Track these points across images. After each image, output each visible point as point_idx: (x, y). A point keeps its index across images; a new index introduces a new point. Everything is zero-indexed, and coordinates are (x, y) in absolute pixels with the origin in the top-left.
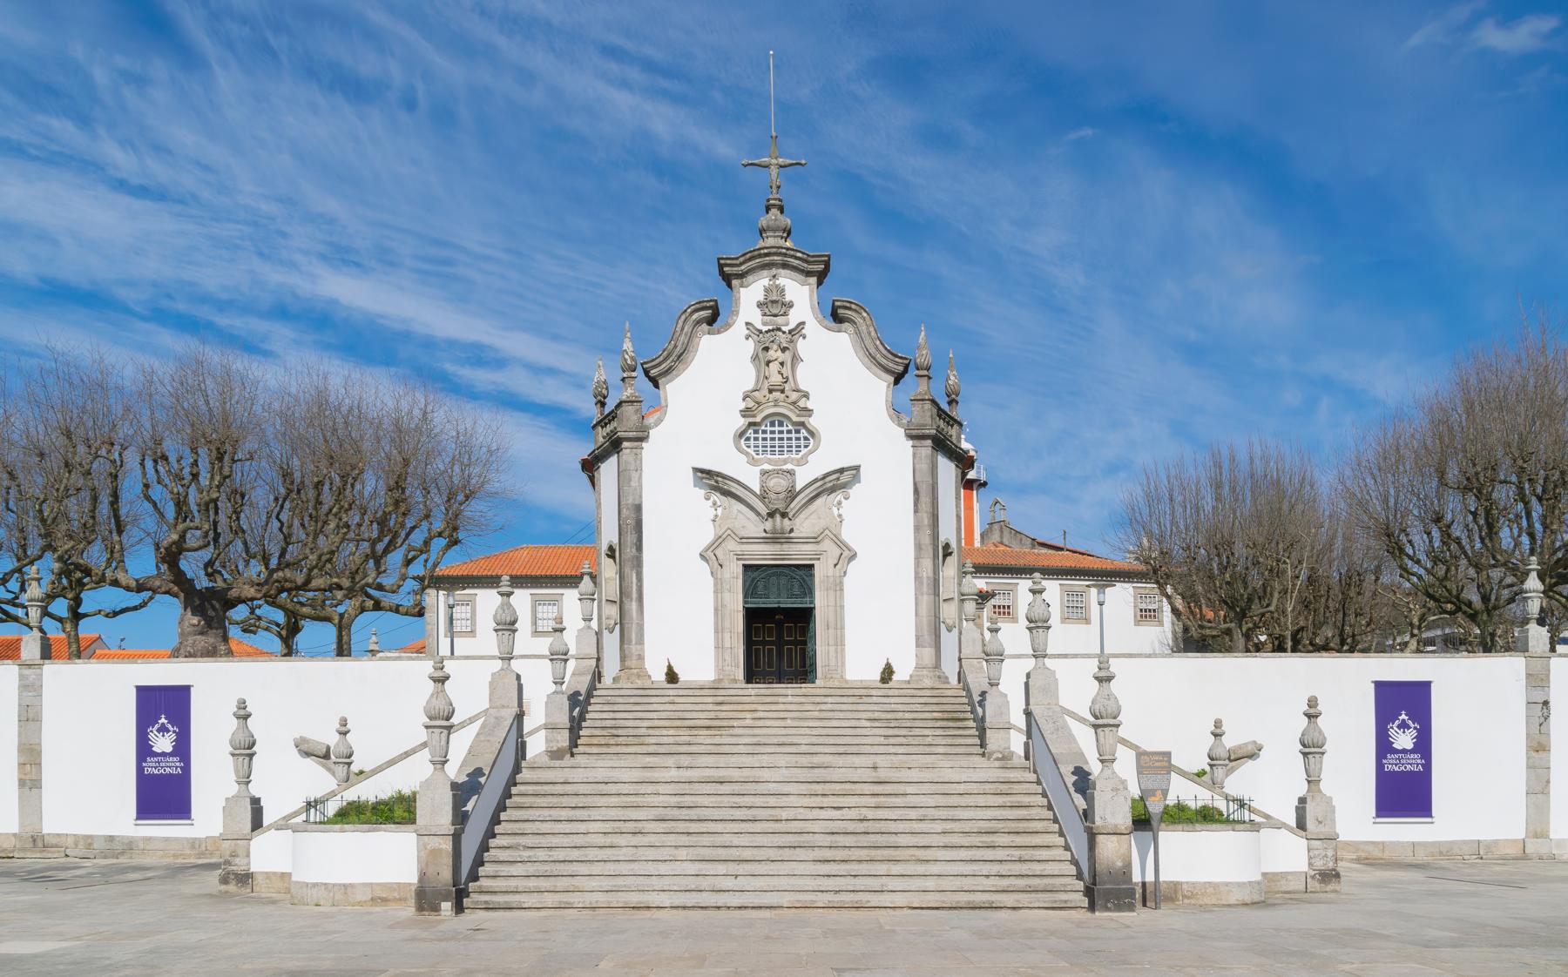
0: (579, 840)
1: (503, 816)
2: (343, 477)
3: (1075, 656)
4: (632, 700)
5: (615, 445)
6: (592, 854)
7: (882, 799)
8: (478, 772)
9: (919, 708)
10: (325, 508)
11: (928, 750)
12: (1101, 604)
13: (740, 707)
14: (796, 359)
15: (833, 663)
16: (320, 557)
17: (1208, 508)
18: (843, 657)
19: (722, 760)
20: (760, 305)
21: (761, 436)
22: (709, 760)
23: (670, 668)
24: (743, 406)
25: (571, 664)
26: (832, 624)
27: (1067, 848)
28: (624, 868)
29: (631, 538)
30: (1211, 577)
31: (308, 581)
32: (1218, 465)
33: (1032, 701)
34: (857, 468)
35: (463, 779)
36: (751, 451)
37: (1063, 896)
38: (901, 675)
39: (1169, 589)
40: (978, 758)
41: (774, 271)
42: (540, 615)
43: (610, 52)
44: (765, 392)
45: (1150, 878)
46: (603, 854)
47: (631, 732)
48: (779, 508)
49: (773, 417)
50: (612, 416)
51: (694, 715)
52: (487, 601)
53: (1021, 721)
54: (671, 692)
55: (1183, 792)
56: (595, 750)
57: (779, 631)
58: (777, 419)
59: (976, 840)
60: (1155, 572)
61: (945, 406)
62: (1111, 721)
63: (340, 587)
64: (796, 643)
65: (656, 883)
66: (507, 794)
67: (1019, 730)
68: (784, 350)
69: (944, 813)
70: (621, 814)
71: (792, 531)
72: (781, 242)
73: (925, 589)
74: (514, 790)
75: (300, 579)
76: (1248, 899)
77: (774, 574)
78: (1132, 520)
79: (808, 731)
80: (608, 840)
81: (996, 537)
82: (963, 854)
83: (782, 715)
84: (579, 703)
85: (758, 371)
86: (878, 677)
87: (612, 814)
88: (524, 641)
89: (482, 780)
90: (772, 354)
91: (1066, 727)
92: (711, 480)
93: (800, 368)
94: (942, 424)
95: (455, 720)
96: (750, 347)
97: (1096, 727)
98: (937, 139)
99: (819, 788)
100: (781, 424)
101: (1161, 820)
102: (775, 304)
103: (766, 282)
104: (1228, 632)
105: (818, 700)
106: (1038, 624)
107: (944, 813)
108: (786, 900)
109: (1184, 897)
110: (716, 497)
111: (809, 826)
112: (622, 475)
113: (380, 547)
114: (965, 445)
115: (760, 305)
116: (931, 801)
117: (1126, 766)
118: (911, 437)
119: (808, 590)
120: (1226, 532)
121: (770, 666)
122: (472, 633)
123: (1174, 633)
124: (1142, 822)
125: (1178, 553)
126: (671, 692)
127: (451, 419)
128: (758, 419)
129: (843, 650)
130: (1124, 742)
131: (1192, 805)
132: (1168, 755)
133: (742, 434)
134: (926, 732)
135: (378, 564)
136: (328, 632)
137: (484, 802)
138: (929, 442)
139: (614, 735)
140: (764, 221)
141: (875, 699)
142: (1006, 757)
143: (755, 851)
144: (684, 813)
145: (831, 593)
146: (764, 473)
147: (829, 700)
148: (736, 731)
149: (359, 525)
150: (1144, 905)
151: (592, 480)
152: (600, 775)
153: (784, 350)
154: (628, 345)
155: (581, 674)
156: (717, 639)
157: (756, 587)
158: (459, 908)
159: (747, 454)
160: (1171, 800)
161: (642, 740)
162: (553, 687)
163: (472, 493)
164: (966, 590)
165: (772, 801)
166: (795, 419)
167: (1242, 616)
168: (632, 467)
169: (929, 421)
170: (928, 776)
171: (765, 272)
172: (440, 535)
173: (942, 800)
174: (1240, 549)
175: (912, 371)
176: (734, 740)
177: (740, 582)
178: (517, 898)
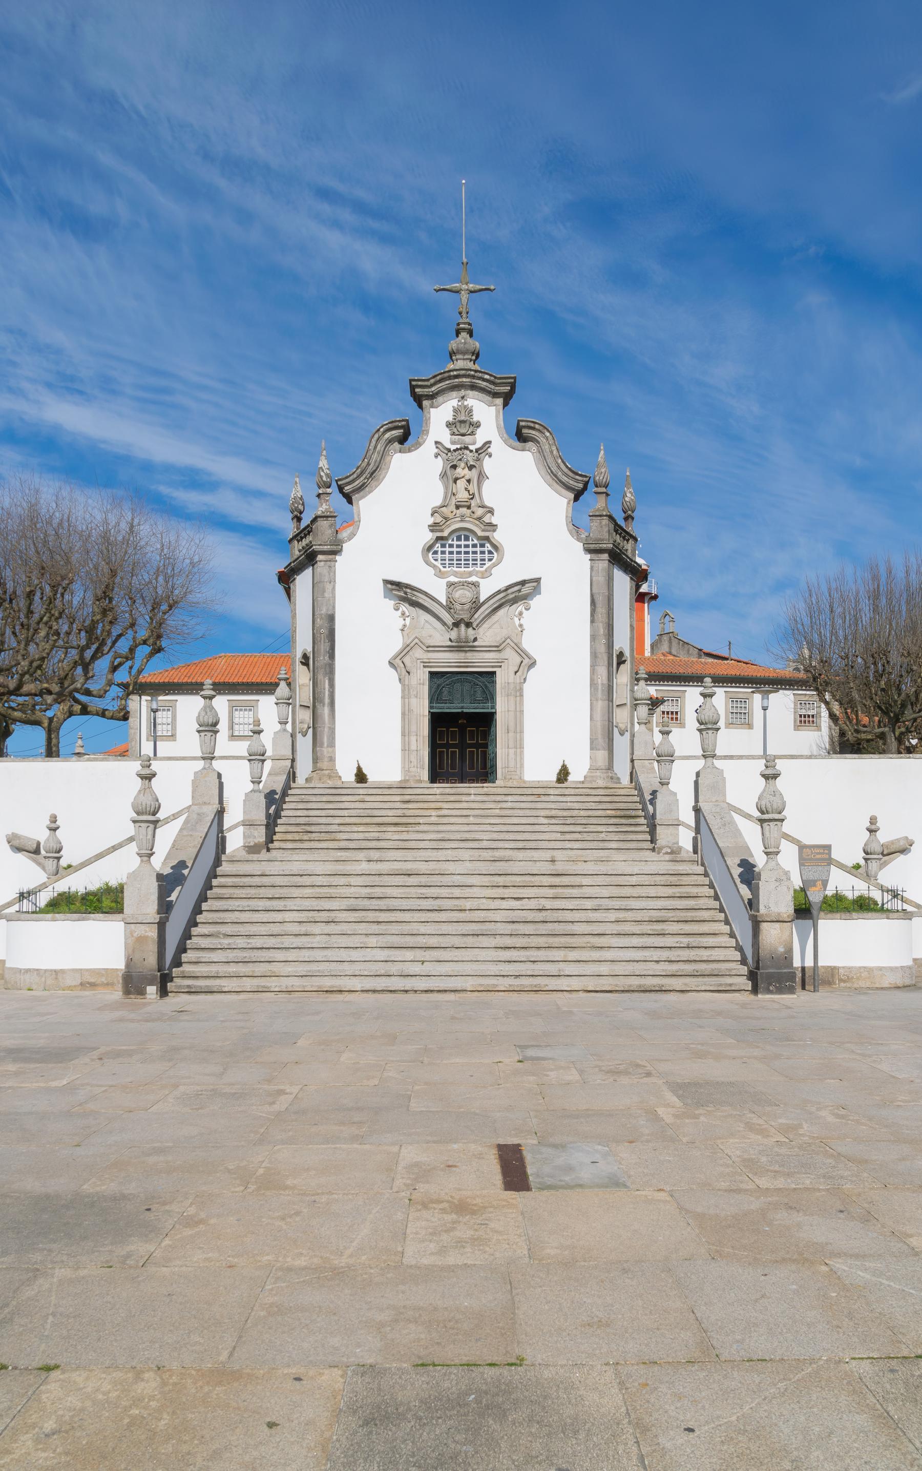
0: (275, 929)
1: (204, 906)
2: (54, 587)
3: (741, 757)
4: (324, 799)
5: (310, 558)
6: (288, 941)
7: (560, 890)
8: (182, 864)
9: (593, 806)
10: (36, 617)
11: (601, 845)
12: (765, 709)
14: (482, 476)
15: (512, 764)
16: (31, 663)
17: (865, 620)
18: (522, 759)
19: (409, 855)
20: (449, 425)
21: (447, 549)
22: (399, 855)
23: (359, 769)
24: (431, 521)
25: (268, 765)
26: (512, 728)
27: (732, 935)
28: (319, 955)
29: (324, 646)
30: (867, 685)
31: (20, 686)
32: (875, 578)
33: (701, 798)
34: (538, 580)
35: (167, 871)
36: (438, 564)
37: (729, 980)
38: (577, 775)
39: (827, 696)
40: (648, 853)
41: (463, 392)
42: (236, 720)
43: (324, 194)
45: (809, 963)
46: (298, 942)
47: (323, 828)
48: (464, 617)
49: (461, 531)
50: (307, 531)
52: (189, 707)
53: (688, 817)
54: (361, 791)
55: (842, 883)
56: (289, 845)
57: (462, 735)
58: (463, 534)
59: (647, 928)
60: (815, 679)
61: (622, 523)
62: (777, 816)
63: (49, 692)
64: (477, 746)
65: (348, 968)
66: (208, 886)
67: (687, 826)
68: (471, 468)
69: (617, 904)
70: (315, 904)
71: (475, 640)
72: (470, 365)
73: (600, 695)
74: (215, 882)
75: (12, 684)
76: (900, 983)
77: (459, 681)
78: (796, 633)
79: (489, 828)
80: (303, 929)
81: (665, 647)
82: (635, 941)
83: (465, 812)
84: (275, 801)
85: (446, 488)
87: (307, 904)
88: (223, 744)
89: (186, 872)
90: (460, 471)
91: (732, 822)
92: (401, 592)
93: (486, 485)
94: (618, 538)
95: (161, 815)
97: (762, 821)
98: (627, 278)
99: (500, 880)
100: (467, 538)
101: (821, 909)
102: (463, 424)
103: (454, 403)
104: (882, 736)
106: (707, 726)
107: (617, 904)
108: (469, 983)
109: (841, 980)
110: (404, 607)
111: (491, 916)
112: (315, 585)
113: (88, 654)
114: (639, 560)
115: (449, 425)
116: (605, 892)
117: (789, 858)
118: (589, 551)
119: (490, 696)
120: (882, 641)
122: (173, 737)
123: (831, 738)
124: (803, 911)
125: (838, 663)
126: (361, 791)
127: (154, 535)
128: (445, 534)
129: (522, 753)
130: (786, 837)
131: (850, 895)
132: (828, 848)
133: (430, 548)
134: (600, 828)
135: (86, 667)
136: (38, 735)
137: (187, 894)
139: (307, 833)
140: (454, 344)
141: (552, 798)
142: (675, 851)
143: (441, 939)
144: (375, 904)
145: (512, 699)
146: (450, 585)
147: (510, 798)
148: (421, 828)
149: (68, 634)
150: (803, 988)
151: (288, 592)
152: (295, 868)
153: (471, 468)
154: (323, 463)
155: (276, 774)
157: (441, 693)
158: (164, 992)
159: (434, 567)
160: (830, 891)
161: (333, 836)
162: (251, 786)
163: (176, 602)
164: (639, 695)
165: (457, 892)
166: (480, 533)
167: (896, 720)
168: (326, 579)
169: (606, 536)
170: (602, 868)
171: (454, 394)
172: (145, 642)
174: (895, 658)
175: (591, 488)
176: (420, 836)
177: (426, 688)
178: (217, 982)
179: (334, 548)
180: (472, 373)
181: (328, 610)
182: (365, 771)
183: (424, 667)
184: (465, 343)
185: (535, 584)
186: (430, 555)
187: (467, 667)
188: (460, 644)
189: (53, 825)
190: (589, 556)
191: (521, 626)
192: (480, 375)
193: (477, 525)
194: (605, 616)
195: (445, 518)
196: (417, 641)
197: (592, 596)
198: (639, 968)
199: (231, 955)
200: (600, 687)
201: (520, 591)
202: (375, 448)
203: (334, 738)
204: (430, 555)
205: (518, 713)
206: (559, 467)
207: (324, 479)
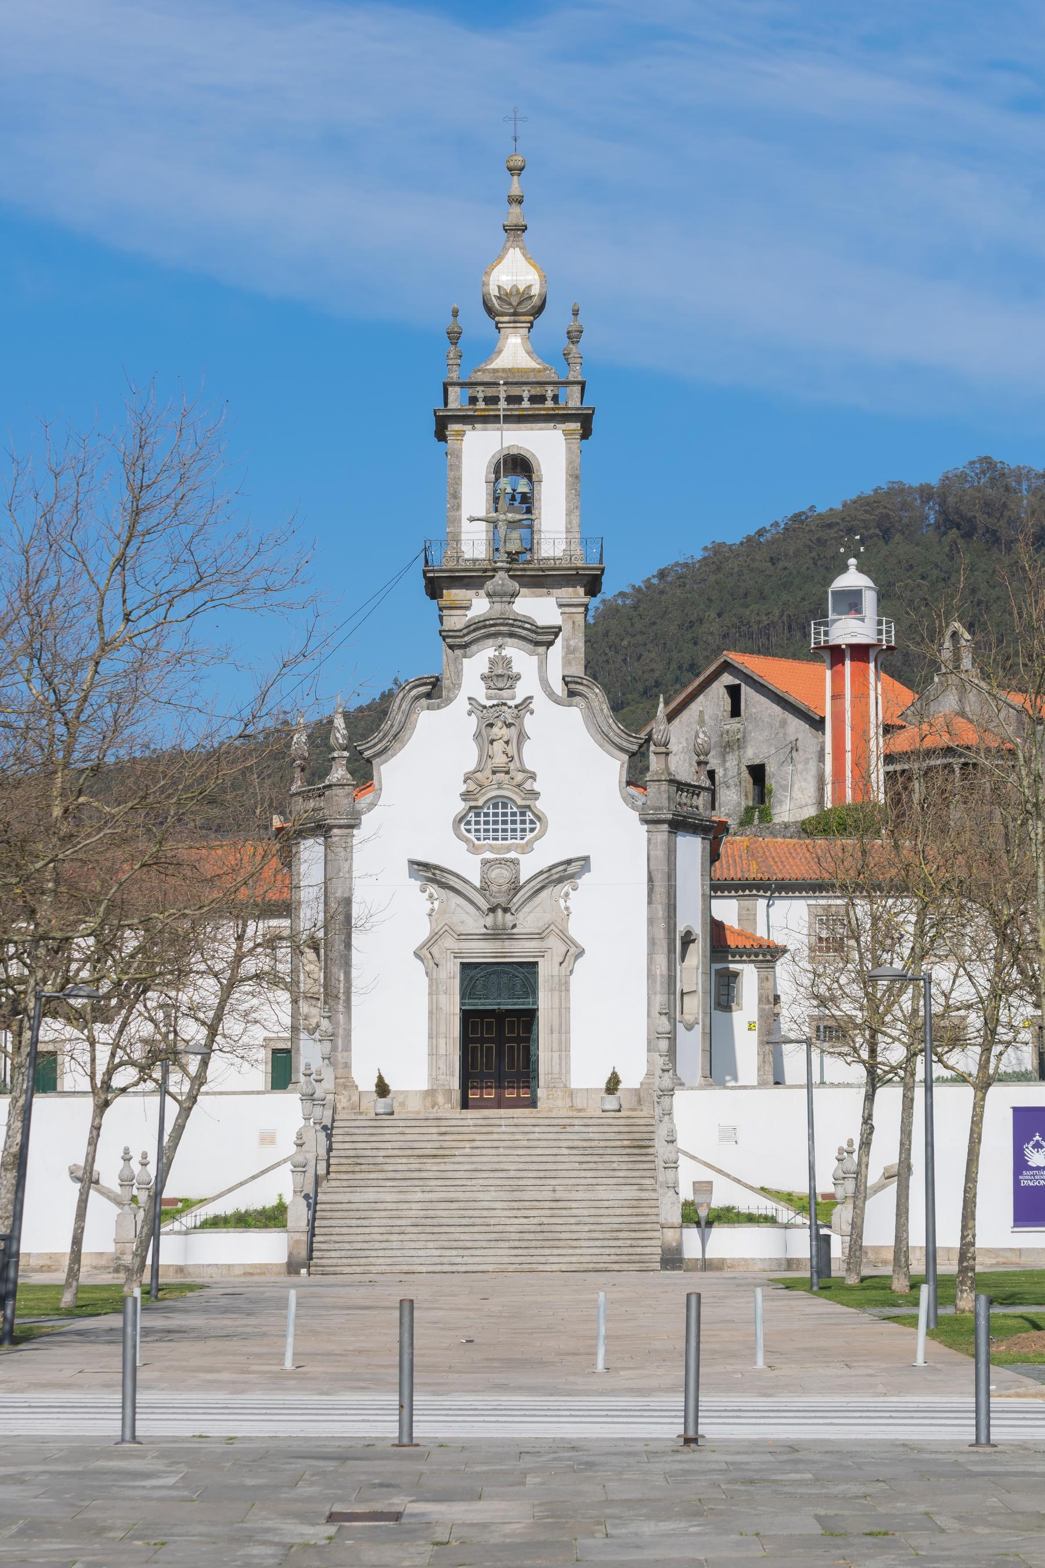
0: (367, 1238)
4: (368, 1131)
7: (556, 1211)
9: (612, 1136)
13: (460, 1137)
14: (522, 737)
15: (556, 1070)
18: (568, 1064)
20: (484, 678)
23: (380, 1078)
24: (463, 788)
26: (556, 1028)
38: (631, 1080)
41: (500, 640)
44: (488, 772)
48: (502, 900)
51: (423, 1145)
57: (498, 1037)
59: (607, 1235)
64: (518, 1040)
71: (514, 926)
73: (658, 988)
79: (517, 1159)
83: (495, 1144)
85: (481, 750)
86: (603, 1085)
87: (384, 1222)
92: (428, 873)
93: (527, 747)
96: (472, 723)
99: (515, 1205)
102: (500, 677)
105: (527, 1129)
108: (491, 1268)
110: (432, 889)
115: (484, 678)
119: (531, 989)
121: (489, 1067)
128: (480, 803)
129: (568, 1057)
138: (665, 827)
144: (429, 1221)
146: (485, 862)
147: (537, 1129)
156: (430, 1046)
161: (380, 1167)
165: (485, 1213)
166: (520, 802)
171: (490, 641)
173: (593, 1212)
177: (457, 981)
179: (352, 822)
180: (511, 622)
181: (343, 892)
182: (387, 1081)
183: (455, 957)
184: (503, 585)
185: (582, 863)
186: (462, 826)
187: (505, 957)
188: (497, 932)
189: (144, 1161)
190: (645, 827)
191: (567, 908)
192: (520, 624)
193: (516, 793)
194: (665, 896)
195: (481, 786)
196: (446, 928)
197: (649, 873)
198: (595, 1259)
199: (343, 1253)
200: (659, 978)
201: (565, 870)
202: (400, 707)
203: (349, 1041)
204: (462, 826)
205: (563, 1011)
206: (610, 726)
207: (341, 741)
